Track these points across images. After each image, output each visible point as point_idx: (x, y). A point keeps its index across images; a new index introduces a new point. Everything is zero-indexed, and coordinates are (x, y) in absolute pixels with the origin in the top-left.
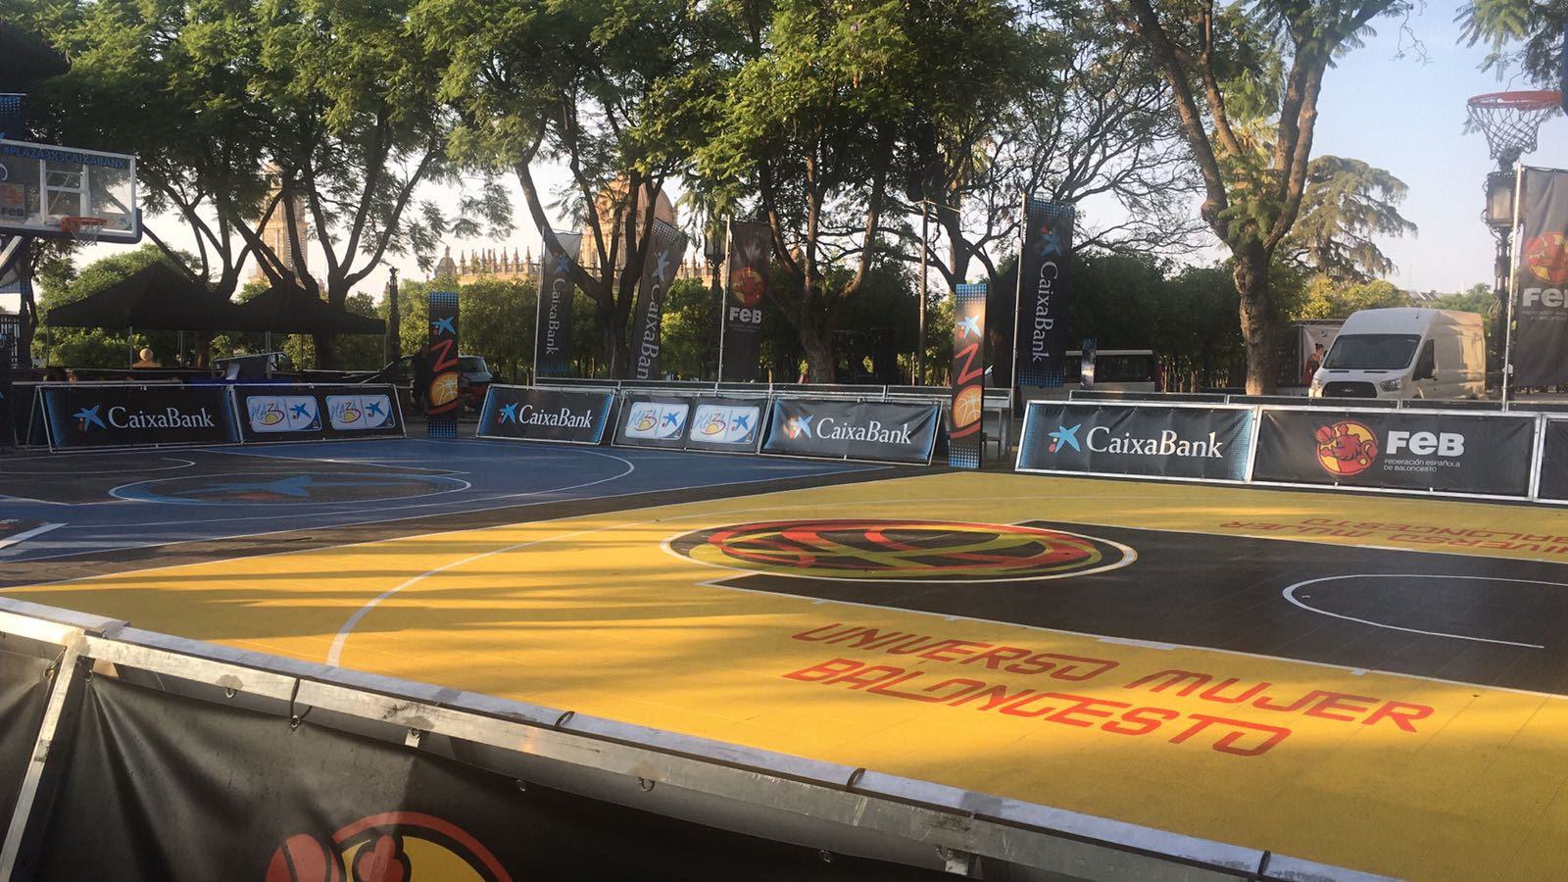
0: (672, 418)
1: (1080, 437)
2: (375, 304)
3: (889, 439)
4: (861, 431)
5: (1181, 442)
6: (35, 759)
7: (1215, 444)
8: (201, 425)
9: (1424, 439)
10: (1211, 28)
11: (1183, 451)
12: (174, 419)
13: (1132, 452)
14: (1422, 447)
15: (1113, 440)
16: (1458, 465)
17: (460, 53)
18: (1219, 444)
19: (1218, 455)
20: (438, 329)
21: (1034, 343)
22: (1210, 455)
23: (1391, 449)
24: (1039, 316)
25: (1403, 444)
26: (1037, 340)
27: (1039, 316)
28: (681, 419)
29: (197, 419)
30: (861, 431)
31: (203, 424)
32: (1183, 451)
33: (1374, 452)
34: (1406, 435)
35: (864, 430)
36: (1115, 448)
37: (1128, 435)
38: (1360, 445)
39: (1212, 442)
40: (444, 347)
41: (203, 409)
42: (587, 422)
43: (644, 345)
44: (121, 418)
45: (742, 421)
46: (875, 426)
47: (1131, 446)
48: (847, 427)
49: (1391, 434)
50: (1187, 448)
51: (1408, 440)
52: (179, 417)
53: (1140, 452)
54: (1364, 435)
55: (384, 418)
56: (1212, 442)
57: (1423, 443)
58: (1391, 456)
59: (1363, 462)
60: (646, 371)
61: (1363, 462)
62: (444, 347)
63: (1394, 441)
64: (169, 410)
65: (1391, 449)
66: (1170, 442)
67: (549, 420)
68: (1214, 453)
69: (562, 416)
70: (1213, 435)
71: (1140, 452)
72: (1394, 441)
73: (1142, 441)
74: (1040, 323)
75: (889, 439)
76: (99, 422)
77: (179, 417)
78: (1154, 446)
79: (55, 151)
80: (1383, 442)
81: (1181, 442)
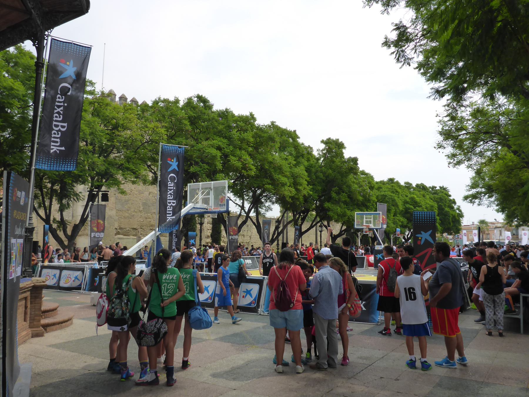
0: (55, 275)
2: (315, 153)
3: (54, 137)
4: (60, 117)
5: (60, 133)
7: (58, 150)
11: (55, 134)
13: (56, 107)
15: (64, 97)
18: (58, 152)
19: (52, 151)
20: (421, 240)
21: (53, 139)
22: (52, 147)
24: (169, 200)
27: (169, 200)
28: (58, 275)
29: (170, 214)
30: (60, 117)
31: (53, 146)
32: (55, 134)
36: (59, 98)
37: (66, 105)
40: (426, 254)
41: (63, 148)
45: (55, 275)
46: (63, 127)
48: (64, 106)
50: (56, 136)
52: (172, 206)
53: (55, 111)
55: (252, 299)
60: (171, 212)
62: (426, 254)
64: (66, 125)
66: (60, 127)
68: (53, 149)
69: (60, 124)
70: (63, 148)
71: (55, 111)
73: (62, 112)
74: (170, 203)
75: (54, 137)
77: (172, 206)
78: (58, 119)
81: (60, 133)
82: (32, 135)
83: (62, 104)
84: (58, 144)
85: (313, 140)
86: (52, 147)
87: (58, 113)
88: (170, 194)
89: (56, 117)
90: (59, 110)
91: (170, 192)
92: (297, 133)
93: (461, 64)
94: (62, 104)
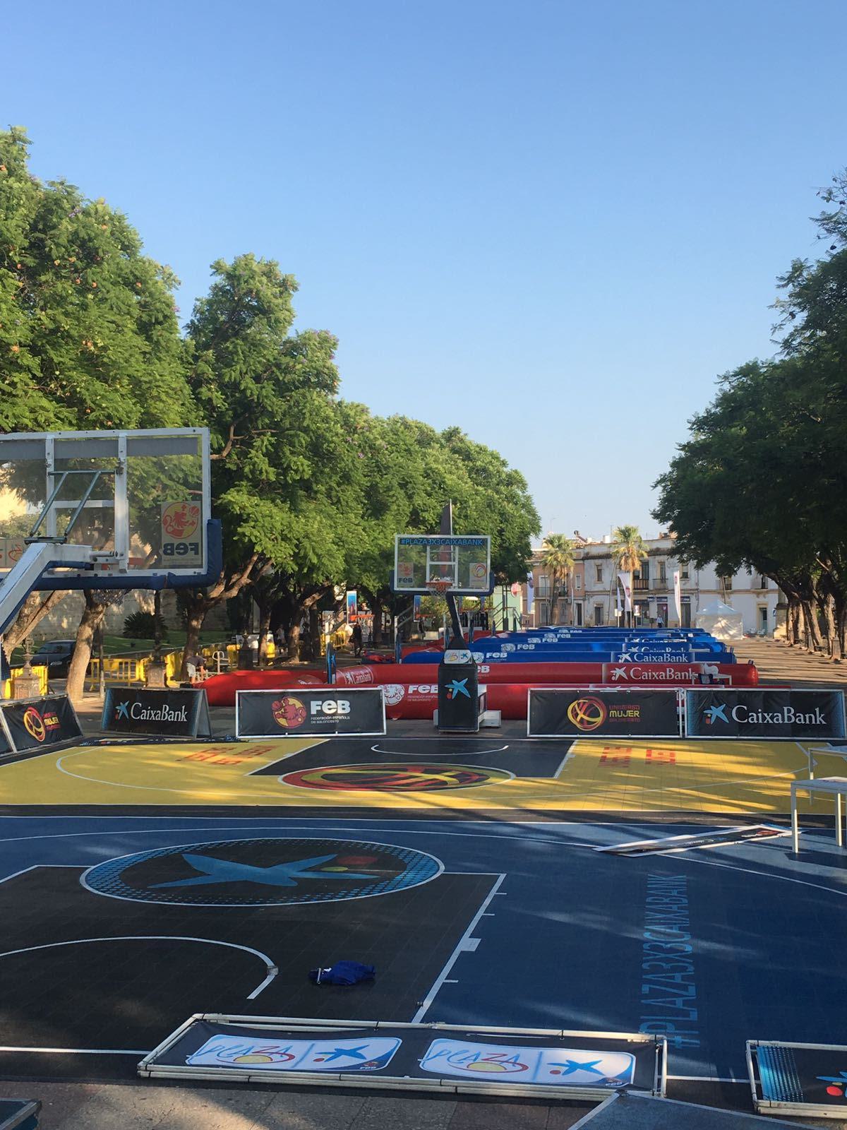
1: (727, 712)
6: (196, 548)
8: (814, 722)
9: (329, 705)
10: (621, 680)
12: (788, 716)
14: (330, 709)
16: (349, 718)
17: (269, 545)
19: (824, 723)
21: (808, 722)
23: (313, 712)
24: (783, 720)
25: (319, 708)
26: (805, 720)
27: (783, 720)
29: (810, 718)
31: (816, 721)
33: (304, 714)
34: (320, 703)
35: (780, 715)
36: (753, 720)
38: (297, 710)
39: (818, 713)
41: (817, 710)
42: (183, 716)
43: (786, 721)
44: (741, 714)
47: (764, 718)
49: (312, 702)
51: (321, 706)
52: (794, 715)
53: (771, 722)
54: (298, 704)
56: (818, 713)
57: (330, 707)
58: (314, 716)
59: (300, 720)
60: (807, 716)
61: (300, 720)
63: (315, 707)
64: (785, 708)
65: (313, 712)
67: (155, 716)
69: (786, 715)
70: (817, 710)
71: (771, 722)
72: (315, 707)
74: (789, 718)
76: (465, 692)
77: (794, 715)
79: (434, 539)
80: (308, 708)
82: (495, 1102)
83: (760, 715)
84: (812, 715)
85: (688, 436)
86: (818, 723)
87: (658, 676)
88: (772, 718)
89: (778, 720)
90: (768, 718)
91: (768, 718)
92: (794, 259)
93: (415, 637)
94: (760, 715)
